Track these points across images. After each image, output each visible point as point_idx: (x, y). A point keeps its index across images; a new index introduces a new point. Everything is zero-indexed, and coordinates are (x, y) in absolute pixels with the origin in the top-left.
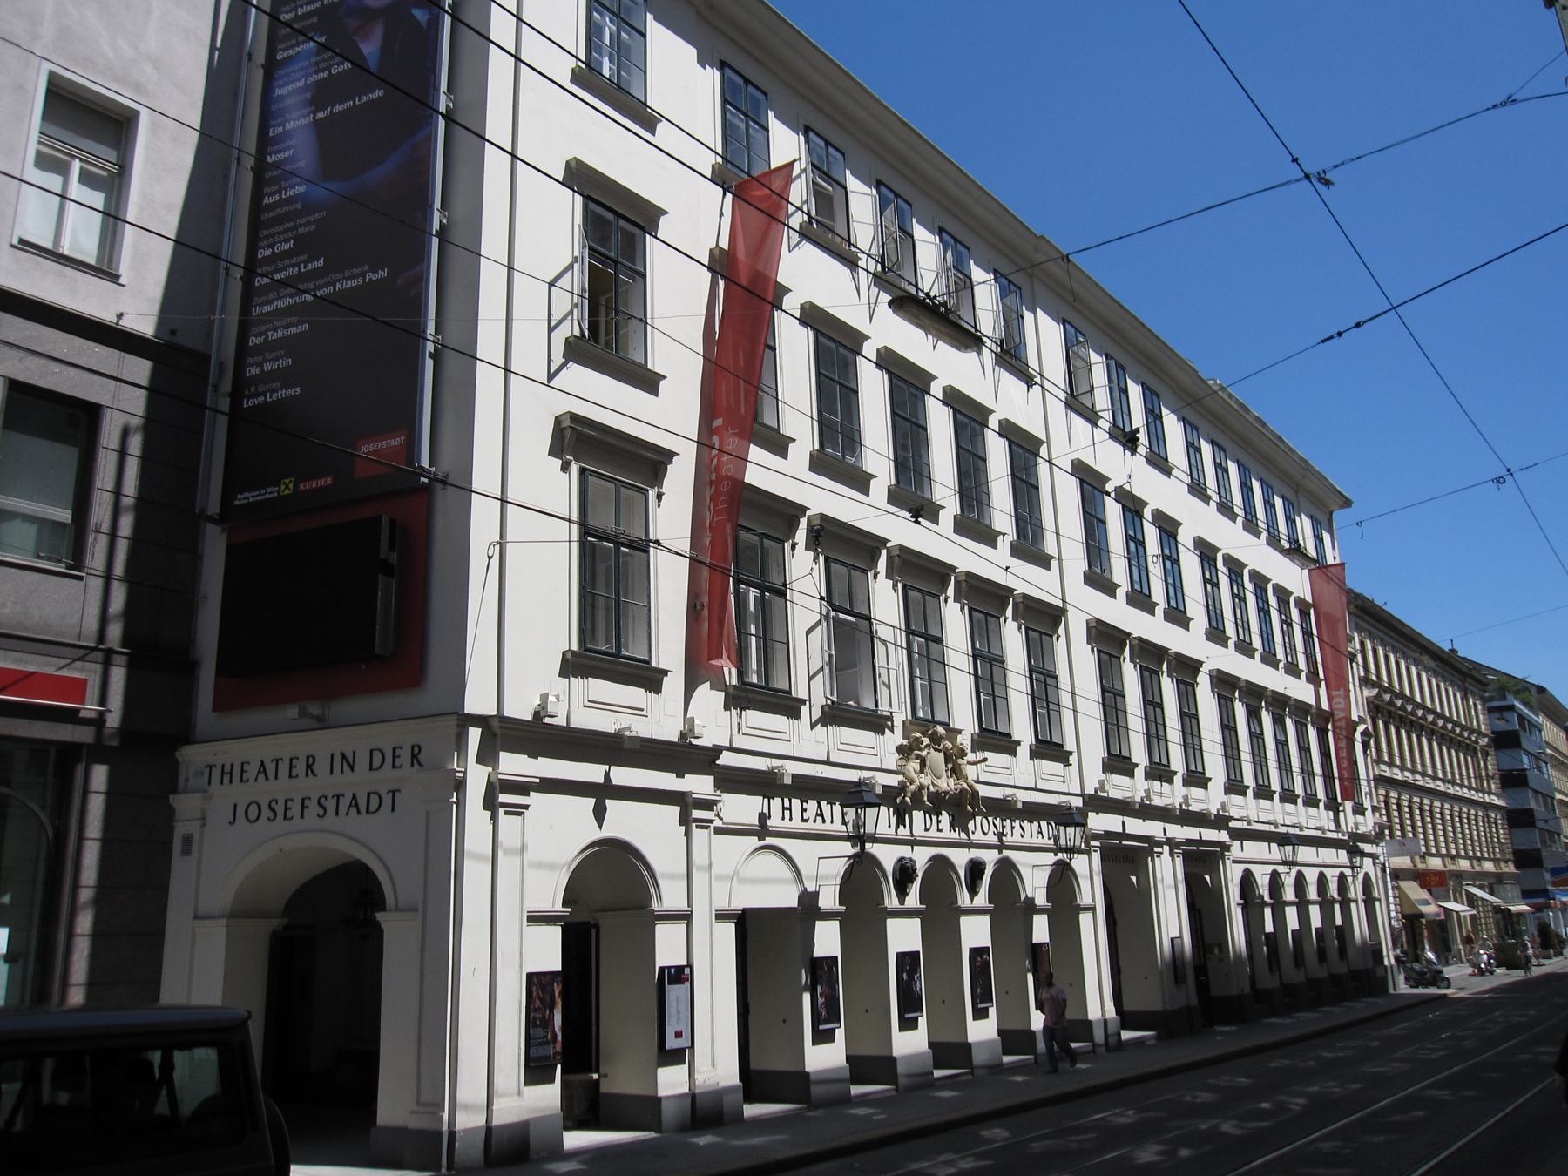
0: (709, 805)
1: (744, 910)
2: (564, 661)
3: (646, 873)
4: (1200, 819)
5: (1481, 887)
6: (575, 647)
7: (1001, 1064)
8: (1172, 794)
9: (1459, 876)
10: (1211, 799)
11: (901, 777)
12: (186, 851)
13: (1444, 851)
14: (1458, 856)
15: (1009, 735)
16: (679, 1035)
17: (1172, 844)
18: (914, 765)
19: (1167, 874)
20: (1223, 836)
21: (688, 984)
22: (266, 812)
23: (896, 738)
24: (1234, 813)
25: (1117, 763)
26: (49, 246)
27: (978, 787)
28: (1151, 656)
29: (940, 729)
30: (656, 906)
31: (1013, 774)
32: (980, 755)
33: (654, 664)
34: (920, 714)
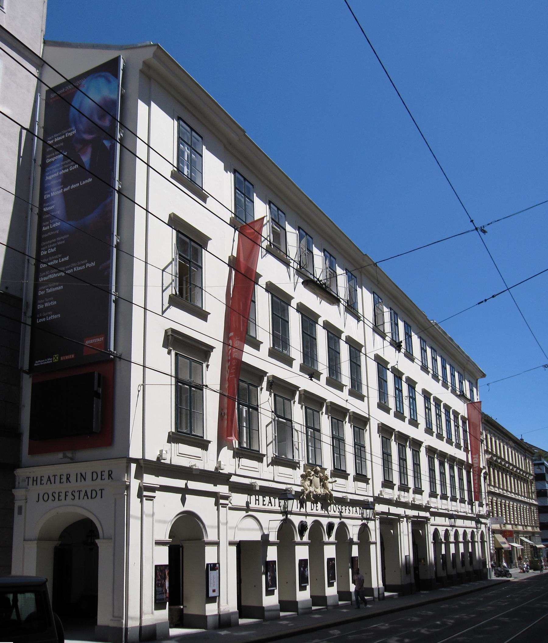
0: (226, 498)
1: (240, 541)
2: (169, 436)
3: (201, 525)
5: (526, 537)
6: (173, 430)
7: (338, 605)
8: (408, 497)
9: (518, 532)
10: (423, 499)
11: (302, 488)
13: (513, 522)
16: (214, 591)
18: (308, 483)
19: (405, 530)
20: (427, 515)
21: (218, 571)
25: (388, 484)
28: (402, 438)
29: (318, 468)
30: (205, 539)
32: (334, 479)
33: (205, 438)
34: (311, 462)
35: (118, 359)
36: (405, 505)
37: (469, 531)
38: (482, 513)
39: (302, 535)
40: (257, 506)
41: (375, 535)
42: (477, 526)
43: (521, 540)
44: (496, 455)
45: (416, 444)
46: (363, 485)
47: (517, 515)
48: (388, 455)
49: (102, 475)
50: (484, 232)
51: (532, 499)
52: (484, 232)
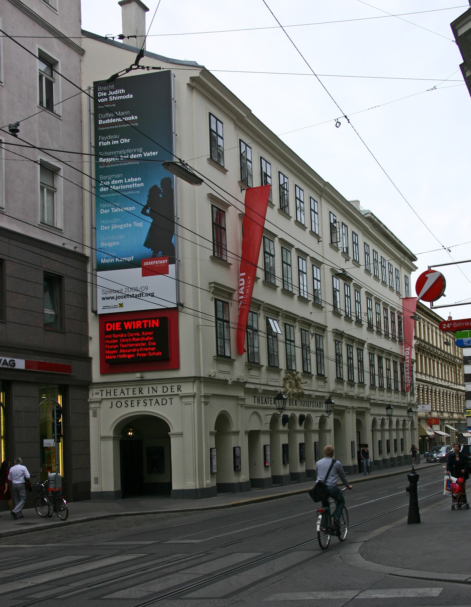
0: (243, 400)
1: (251, 431)
4: (361, 399)
5: (451, 425)
8: (356, 391)
9: (443, 420)
10: (367, 392)
11: (284, 389)
12: (95, 415)
13: (438, 410)
14: (444, 411)
15: (259, 363)
17: (353, 408)
18: (288, 385)
19: (350, 421)
20: (368, 406)
22: (124, 404)
23: (283, 374)
24: (372, 397)
25: (339, 380)
26: (51, 225)
27: (304, 391)
28: (351, 339)
29: (294, 372)
31: (312, 386)
32: (305, 381)
34: (219, 353)
35: (180, 307)
36: (351, 398)
37: (401, 419)
38: (413, 402)
39: (301, 424)
40: (258, 405)
41: (330, 424)
42: (408, 415)
43: (446, 427)
44: (424, 341)
45: (362, 343)
46: (321, 383)
47: (443, 401)
48: (339, 356)
49: (171, 389)
50: (450, 251)
51: (459, 384)
52: (450, 251)
